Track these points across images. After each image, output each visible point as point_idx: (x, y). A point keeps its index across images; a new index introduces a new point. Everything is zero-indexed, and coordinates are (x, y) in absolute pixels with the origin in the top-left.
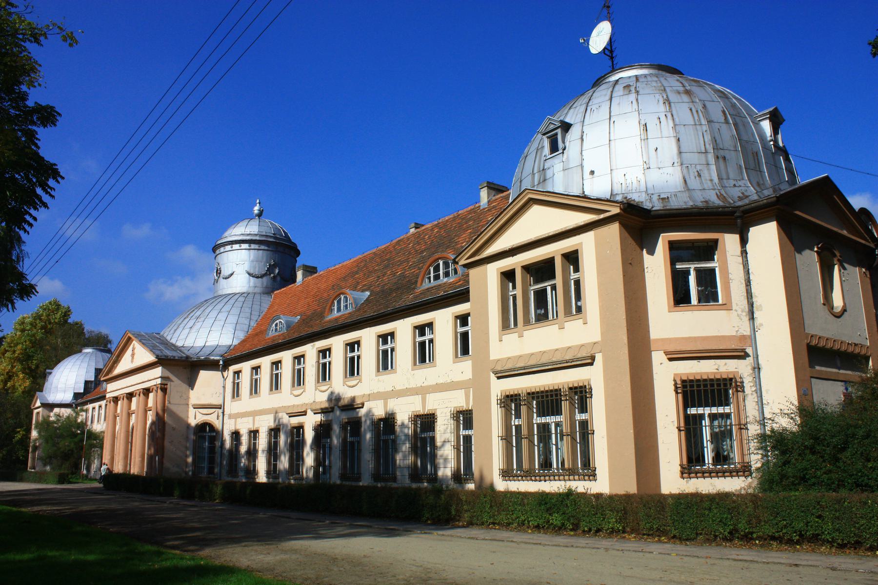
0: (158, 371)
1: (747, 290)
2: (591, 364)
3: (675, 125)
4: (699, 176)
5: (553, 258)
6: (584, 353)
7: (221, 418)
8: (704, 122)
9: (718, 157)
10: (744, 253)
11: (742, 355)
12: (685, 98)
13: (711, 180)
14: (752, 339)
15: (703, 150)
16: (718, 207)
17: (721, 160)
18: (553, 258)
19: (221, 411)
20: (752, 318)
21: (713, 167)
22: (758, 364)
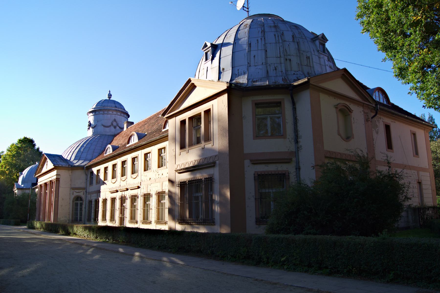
0: (55, 173)
1: (295, 128)
2: (214, 166)
3: (265, 43)
4: (276, 69)
5: (201, 113)
6: (211, 161)
7: (85, 194)
8: (281, 41)
9: (286, 60)
10: (294, 109)
11: (288, 161)
12: (273, 29)
13: (282, 71)
14: (296, 153)
15: (279, 56)
16: (282, 85)
17: (288, 61)
18: (201, 113)
19: (85, 191)
20: (297, 142)
21: (283, 65)
22: (299, 166)
